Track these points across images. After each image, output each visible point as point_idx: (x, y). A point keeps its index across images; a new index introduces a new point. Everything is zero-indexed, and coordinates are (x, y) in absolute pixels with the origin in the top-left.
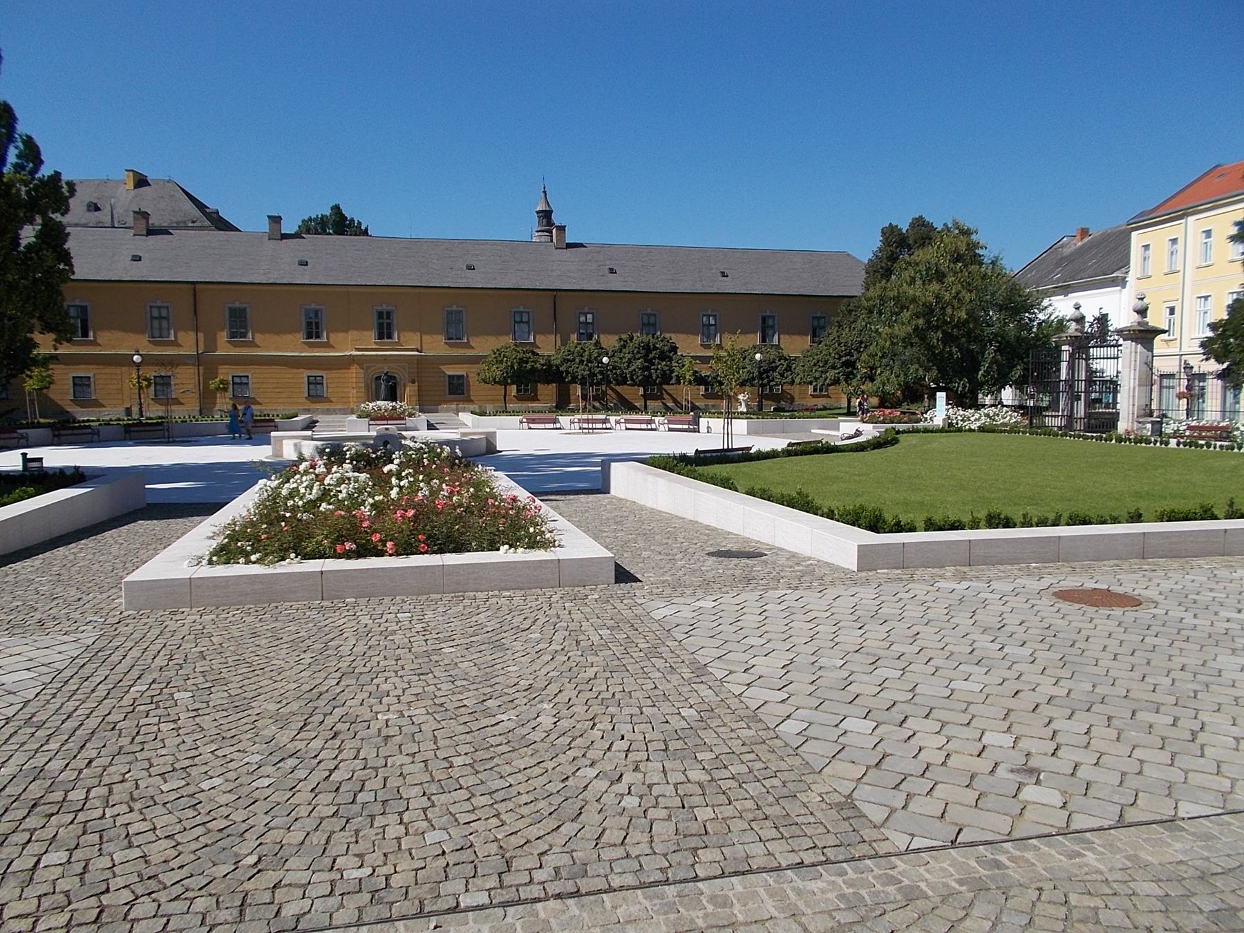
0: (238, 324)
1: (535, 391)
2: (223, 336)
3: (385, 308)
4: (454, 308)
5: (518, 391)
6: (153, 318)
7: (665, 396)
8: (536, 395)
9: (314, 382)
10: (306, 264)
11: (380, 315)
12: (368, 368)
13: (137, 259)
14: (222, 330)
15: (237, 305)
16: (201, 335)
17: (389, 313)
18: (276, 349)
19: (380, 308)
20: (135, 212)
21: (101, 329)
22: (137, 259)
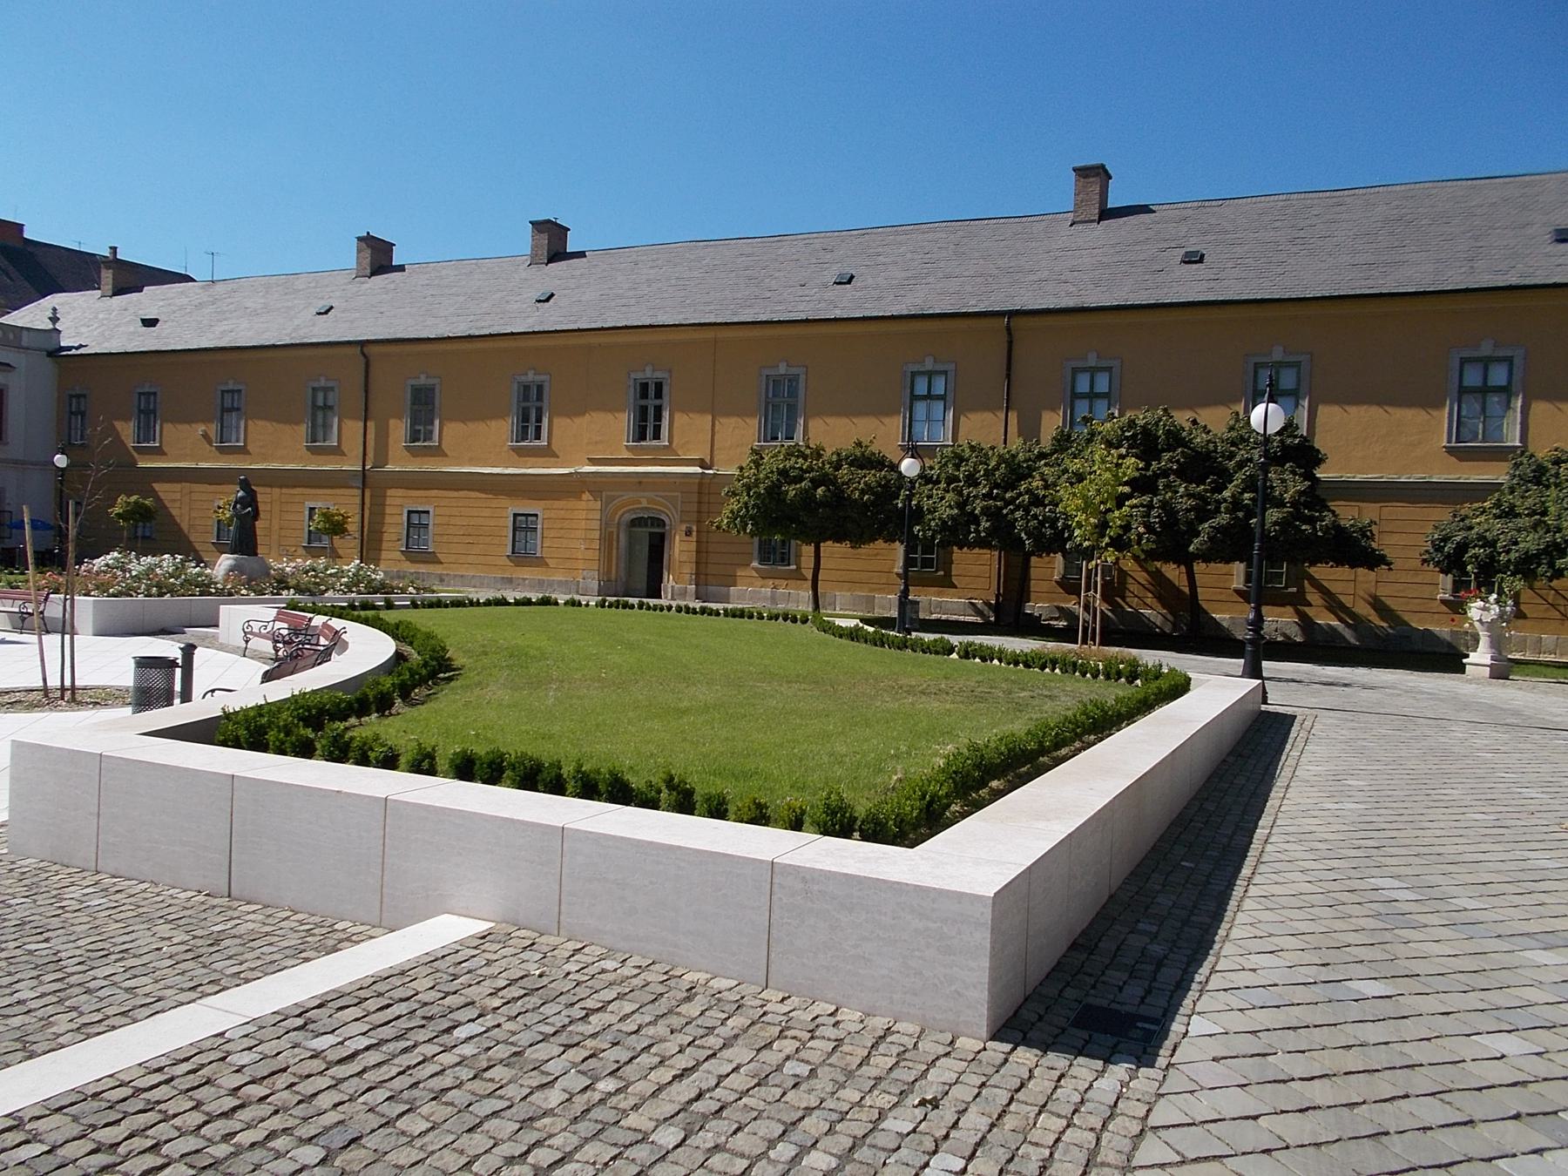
0: (423, 409)
1: (947, 564)
2: (399, 430)
3: (649, 374)
4: (782, 369)
5: (909, 562)
6: (315, 406)
7: (1313, 596)
8: (948, 574)
9: (523, 526)
10: (1201, 261)
11: (644, 389)
12: (611, 499)
13: (150, 323)
14: (1054, 409)
15: (423, 380)
16: (1013, 417)
17: (659, 387)
18: (471, 462)
19: (639, 375)
20: (359, 239)
21: (451, 420)
22: (150, 323)
